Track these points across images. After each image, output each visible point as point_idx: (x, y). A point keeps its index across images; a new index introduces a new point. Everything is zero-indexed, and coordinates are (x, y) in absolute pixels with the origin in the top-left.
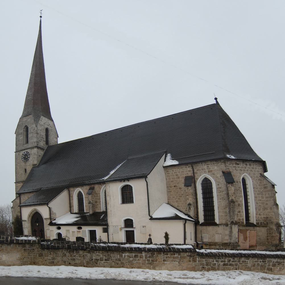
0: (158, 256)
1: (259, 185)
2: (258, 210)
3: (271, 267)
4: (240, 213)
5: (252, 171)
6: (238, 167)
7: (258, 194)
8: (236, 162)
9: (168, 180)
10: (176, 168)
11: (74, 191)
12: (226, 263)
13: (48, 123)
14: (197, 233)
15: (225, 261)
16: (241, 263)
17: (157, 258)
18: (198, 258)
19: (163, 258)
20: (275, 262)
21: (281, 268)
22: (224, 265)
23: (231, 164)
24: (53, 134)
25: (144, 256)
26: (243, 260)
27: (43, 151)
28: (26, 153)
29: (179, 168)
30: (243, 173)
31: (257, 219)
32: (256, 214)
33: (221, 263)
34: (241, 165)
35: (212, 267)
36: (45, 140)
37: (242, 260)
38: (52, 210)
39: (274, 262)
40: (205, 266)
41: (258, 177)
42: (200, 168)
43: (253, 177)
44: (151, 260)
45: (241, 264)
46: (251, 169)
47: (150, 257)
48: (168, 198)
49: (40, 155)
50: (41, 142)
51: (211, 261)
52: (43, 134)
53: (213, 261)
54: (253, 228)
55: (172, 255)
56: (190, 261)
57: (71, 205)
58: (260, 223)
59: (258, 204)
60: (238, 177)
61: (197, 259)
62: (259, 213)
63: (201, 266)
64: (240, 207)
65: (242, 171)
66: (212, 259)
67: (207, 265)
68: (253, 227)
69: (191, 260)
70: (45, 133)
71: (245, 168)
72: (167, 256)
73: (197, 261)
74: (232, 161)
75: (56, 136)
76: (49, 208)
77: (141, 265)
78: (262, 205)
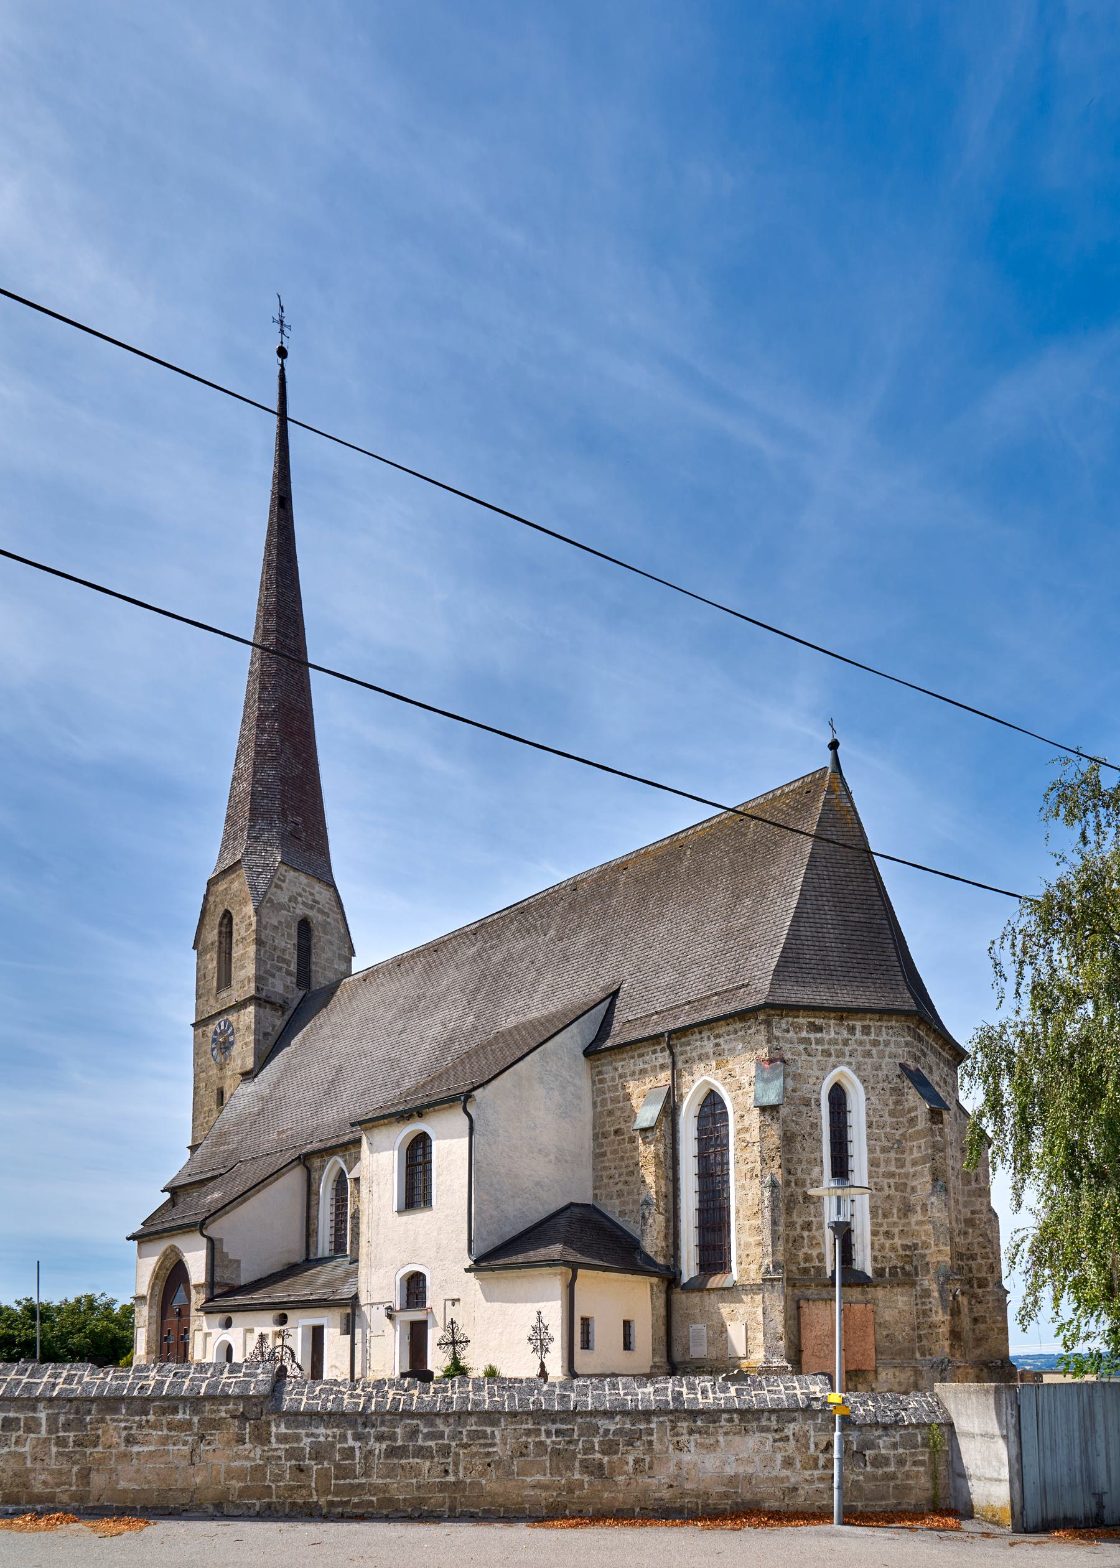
0: (102, 1420)
1: (892, 1114)
2: (880, 1216)
3: (598, 1456)
4: (809, 1231)
5: (868, 1054)
6: (819, 1042)
7: (884, 1150)
8: (812, 1020)
9: (599, 1109)
10: (625, 1056)
11: (323, 1168)
12: (399, 1443)
13: (312, 894)
14: (673, 1323)
15: (393, 1437)
16: (465, 1440)
17: (100, 1432)
18: (278, 1426)
19: (125, 1428)
20: (615, 1433)
21: (643, 1459)
22: (392, 1452)
23: (791, 1028)
24: (331, 943)
25: (44, 1422)
26: (474, 1428)
27: (283, 1013)
28: (222, 1028)
29: (633, 1057)
30: (834, 1067)
31: (877, 1253)
32: (874, 1233)
33: (378, 1445)
34: (828, 1033)
35: (338, 1467)
36: (293, 967)
37: (468, 1428)
38: (225, 1250)
39: (607, 1431)
40: (307, 1462)
41: (890, 1078)
42: (694, 1054)
43: (872, 1081)
44: (71, 1439)
45: (465, 1446)
46: (868, 1047)
47: (67, 1426)
48: (594, 1181)
49: (270, 1030)
50: (273, 976)
51: (334, 1437)
52: (283, 944)
53: (344, 1438)
54: (864, 1293)
55: (164, 1414)
56: (241, 1440)
57: (312, 1227)
58: (887, 1270)
59: (881, 1190)
60: (811, 1081)
61: (274, 1429)
62: (885, 1228)
63: (288, 1464)
64: (812, 1207)
65: (830, 1055)
66: (337, 1427)
67: (316, 1459)
68: (859, 1289)
69: (247, 1436)
70: (295, 941)
71: (846, 1043)
72: (144, 1418)
73: (273, 1440)
74: (798, 1017)
75: (345, 952)
76: (210, 1240)
77: (29, 1464)
78: (899, 1194)
